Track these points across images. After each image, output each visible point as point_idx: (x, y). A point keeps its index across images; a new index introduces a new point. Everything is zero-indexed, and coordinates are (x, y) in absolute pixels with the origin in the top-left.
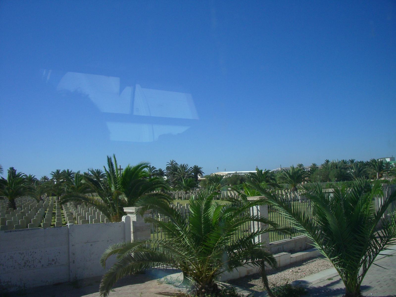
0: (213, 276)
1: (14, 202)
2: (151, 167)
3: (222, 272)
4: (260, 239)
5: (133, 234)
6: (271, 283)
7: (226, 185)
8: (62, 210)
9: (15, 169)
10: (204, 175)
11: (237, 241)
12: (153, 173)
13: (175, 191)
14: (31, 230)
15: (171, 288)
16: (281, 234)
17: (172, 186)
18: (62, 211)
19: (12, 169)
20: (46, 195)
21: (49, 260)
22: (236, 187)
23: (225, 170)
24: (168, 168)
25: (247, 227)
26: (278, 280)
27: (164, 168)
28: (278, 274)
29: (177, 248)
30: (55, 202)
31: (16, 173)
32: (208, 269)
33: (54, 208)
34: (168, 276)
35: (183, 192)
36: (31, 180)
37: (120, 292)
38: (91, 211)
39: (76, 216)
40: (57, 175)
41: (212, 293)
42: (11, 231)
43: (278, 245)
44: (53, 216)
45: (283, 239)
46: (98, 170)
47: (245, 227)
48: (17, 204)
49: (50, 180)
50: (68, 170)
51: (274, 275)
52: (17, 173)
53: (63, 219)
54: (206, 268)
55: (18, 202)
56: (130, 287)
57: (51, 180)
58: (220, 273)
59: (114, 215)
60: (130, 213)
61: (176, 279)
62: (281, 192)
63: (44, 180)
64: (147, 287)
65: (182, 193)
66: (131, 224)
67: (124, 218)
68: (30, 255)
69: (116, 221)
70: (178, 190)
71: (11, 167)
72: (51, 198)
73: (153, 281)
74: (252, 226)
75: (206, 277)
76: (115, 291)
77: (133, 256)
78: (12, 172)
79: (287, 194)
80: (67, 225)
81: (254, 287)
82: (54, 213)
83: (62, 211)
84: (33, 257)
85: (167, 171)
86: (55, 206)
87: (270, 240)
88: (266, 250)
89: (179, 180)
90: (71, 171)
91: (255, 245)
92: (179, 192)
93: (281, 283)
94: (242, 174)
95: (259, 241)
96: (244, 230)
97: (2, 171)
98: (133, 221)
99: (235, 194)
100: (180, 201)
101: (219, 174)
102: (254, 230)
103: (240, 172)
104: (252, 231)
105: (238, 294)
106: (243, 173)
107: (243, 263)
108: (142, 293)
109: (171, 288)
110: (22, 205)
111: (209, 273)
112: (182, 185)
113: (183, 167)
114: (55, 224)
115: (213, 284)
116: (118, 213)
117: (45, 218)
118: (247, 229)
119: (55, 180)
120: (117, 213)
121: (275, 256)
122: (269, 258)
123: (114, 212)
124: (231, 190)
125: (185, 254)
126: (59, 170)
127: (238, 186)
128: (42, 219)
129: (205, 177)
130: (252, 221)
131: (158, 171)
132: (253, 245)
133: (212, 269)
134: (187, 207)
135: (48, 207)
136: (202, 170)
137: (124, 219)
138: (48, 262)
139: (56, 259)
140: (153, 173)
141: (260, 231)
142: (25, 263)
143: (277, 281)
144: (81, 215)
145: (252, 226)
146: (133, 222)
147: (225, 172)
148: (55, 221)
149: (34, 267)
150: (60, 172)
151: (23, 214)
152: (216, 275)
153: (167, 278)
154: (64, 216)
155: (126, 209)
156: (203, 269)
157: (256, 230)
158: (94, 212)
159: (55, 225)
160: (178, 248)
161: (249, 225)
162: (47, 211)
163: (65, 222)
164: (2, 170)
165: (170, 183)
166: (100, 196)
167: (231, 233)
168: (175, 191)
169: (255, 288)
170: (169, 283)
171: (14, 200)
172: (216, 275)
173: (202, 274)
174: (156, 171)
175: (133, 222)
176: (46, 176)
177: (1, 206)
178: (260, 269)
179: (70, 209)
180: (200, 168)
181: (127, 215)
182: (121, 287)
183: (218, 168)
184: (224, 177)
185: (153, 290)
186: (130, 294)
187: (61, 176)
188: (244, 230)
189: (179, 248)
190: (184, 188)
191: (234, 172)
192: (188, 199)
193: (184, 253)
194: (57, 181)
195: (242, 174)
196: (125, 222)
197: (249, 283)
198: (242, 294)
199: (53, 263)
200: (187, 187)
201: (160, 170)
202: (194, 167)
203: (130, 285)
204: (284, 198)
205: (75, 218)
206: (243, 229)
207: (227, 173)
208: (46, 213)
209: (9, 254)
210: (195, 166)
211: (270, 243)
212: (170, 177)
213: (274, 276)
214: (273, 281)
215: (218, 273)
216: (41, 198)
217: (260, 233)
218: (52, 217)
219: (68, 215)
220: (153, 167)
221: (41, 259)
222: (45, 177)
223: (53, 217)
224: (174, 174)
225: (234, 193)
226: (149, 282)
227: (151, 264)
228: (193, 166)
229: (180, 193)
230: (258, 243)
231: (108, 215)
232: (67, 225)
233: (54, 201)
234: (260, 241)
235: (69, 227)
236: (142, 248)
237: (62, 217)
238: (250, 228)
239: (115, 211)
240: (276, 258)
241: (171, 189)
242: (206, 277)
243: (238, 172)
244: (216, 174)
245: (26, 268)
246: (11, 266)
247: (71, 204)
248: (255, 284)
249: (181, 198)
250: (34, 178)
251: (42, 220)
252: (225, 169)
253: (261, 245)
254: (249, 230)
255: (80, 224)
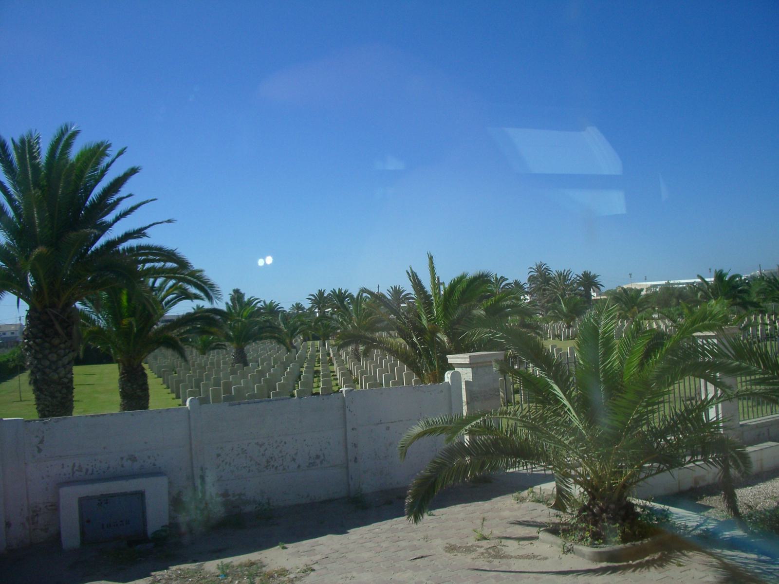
0: (624, 486)
1: (243, 352)
2: (499, 277)
3: (643, 479)
4: (720, 411)
5: (466, 406)
6: (745, 504)
7: (649, 308)
8: (331, 365)
9: (242, 291)
10: (603, 290)
11: (672, 417)
12: (504, 289)
13: (548, 323)
14: (276, 400)
15: (542, 511)
16: (763, 403)
17: (541, 314)
18: (331, 368)
19: (237, 291)
20: (302, 338)
21: (310, 457)
22: (669, 312)
23: (646, 279)
24: (531, 279)
25: (693, 391)
26: (759, 498)
27: (524, 279)
28: (759, 485)
29: (555, 427)
30: (318, 351)
31: (244, 299)
32: (615, 472)
33: (316, 363)
34: (535, 487)
35: (562, 324)
36: (272, 310)
37: (443, 517)
38: (386, 367)
39: (357, 375)
40: (320, 300)
41: (624, 520)
42: (239, 404)
43: (757, 426)
44: (316, 377)
45: (767, 415)
46: (395, 287)
47: (689, 391)
48: (249, 357)
49: (307, 310)
50: (340, 290)
51: (750, 488)
52: (246, 299)
53: (334, 383)
54: (611, 470)
55: (251, 353)
56: (462, 507)
57: (309, 309)
58: (638, 481)
59: (429, 370)
60: (461, 366)
61: (550, 493)
62: (762, 318)
63: (296, 310)
64: (496, 507)
65: (560, 327)
66: (462, 387)
67: (449, 376)
68: (276, 448)
69: (435, 382)
70: (552, 322)
71: (236, 288)
72: (310, 343)
73: (506, 496)
74: (703, 389)
75: (611, 487)
76: (434, 515)
77: (467, 446)
78: (237, 296)
79: (775, 323)
80: (342, 391)
81: (710, 511)
82: (318, 372)
83: (331, 368)
84: (281, 452)
85: (530, 285)
86: (319, 358)
87: (741, 416)
88: (732, 437)
89: (554, 301)
90: (346, 292)
91: (709, 424)
92: (554, 325)
93: (766, 505)
94: (681, 286)
95: (717, 415)
96: (685, 397)
97: (219, 296)
98: (465, 381)
99: (666, 327)
100: (557, 342)
101: (633, 288)
102: (707, 396)
103: (677, 281)
104: (703, 397)
105: (674, 523)
106: (683, 284)
107: (685, 460)
108: (484, 519)
109: (542, 511)
110: (259, 357)
111: (616, 481)
112: (561, 311)
113: (563, 277)
114: (320, 392)
115: (625, 503)
116: (436, 367)
117: (300, 380)
118: (693, 395)
119: (315, 309)
120: (435, 367)
121: (749, 449)
122: (739, 453)
123: (429, 365)
124: (659, 319)
125: (569, 441)
126: (323, 291)
127: (672, 309)
128: (296, 383)
129: (607, 293)
130: (703, 378)
131: (513, 285)
132: (704, 425)
133: (622, 472)
134: (572, 353)
135: (306, 361)
136: (598, 280)
137: (448, 378)
138: (309, 460)
139: (324, 455)
140: (504, 289)
141: (720, 395)
142: (268, 462)
143: (758, 500)
144: (368, 374)
145: (703, 389)
146: (467, 383)
147: (646, 282)
148: (318, 387)
149: (284, 469)
150: (326, 295)
151: (262, 373)
152: (631, 484)
153: (534, 490)
154: (336, 376)
155: (452, 359)
156: (604, 472)
157: (710, 396)
158: (393, 366)
159: (319, 393)
160: (556, 428)
161: (697, 386)
162: (303, 367)
163: (337, 387)
164: (220, 295)
165: (537, 307)
166: (401, 337)
167: (660, 400)
168: (548, 323)
169: (710, 514)
170: (538, 501)
171: (243, 349)
172: (631, 484)
173: (604, 482)
174: (509, 284)
175: (467, 383)
176: (299, 303)
177: (221, 361)
178: (720, 474)
179: (346, 364)
180: (595, 276)
181: (454, 370)
182: (446, 507)
183: (630, 275)
184: (644, 293)
185: (506, 513)
186: (464, 520)
187: (327, 301)
188: (685, 397)
189: (558, 428)
190: (566, 316)
191: (664, 282)
192: (574, 339)
193: (567, 439)
194: (321, 312)
195: (681, 286)
196: (450, 383)
197: (699, 502)
198: (684, 524)
199: (318, 461)
200: (570, 314)
201: (517, 283)
202: (582, 275)
203: (463, 505)
204: (769, 331)
205: (356, 380)
206: (685, 394)
207: (649, 284)
208: (302, 372)
209: (238, 445)
210: (584, 272)
211: (741, 423)
212: (536, 296)
213: (749, 491)
214: (748, 500)
215: (634, 481)
216: (291, 343)
217: (720, 400)
218: (313, 380)
219: (343, 375)
220: (502, 277)
221: (296, 454)
222: (297, 304)
223: (316, 380)
224: (544, 290)
225: (665, 324)
226: (498, 498)
227: (502, 464)
228: (580, 273)
229: (557, 328)
230: (715, 419)
231: (419, 374)
232: (342, 391)
233: (317, 349)
234: (720, 416)
235: (344, 395)
236: (487, 429)
237: (333, 378)
238: (699, 394)
239: (431, 363)
240: (751, 455)
241: (539, 319)
242: (611, 487)
243: (671, 282)
244: (625, 287)
245: (270, 470)
246: (244, 467)
247: (347, 354)
248: (710, 505)
249: (559, 336)
250: (278, 307)
251: (296, 385)
252: (646, 277)
253: (721, 425)
254: (697, 396)
255: (366, 388)
